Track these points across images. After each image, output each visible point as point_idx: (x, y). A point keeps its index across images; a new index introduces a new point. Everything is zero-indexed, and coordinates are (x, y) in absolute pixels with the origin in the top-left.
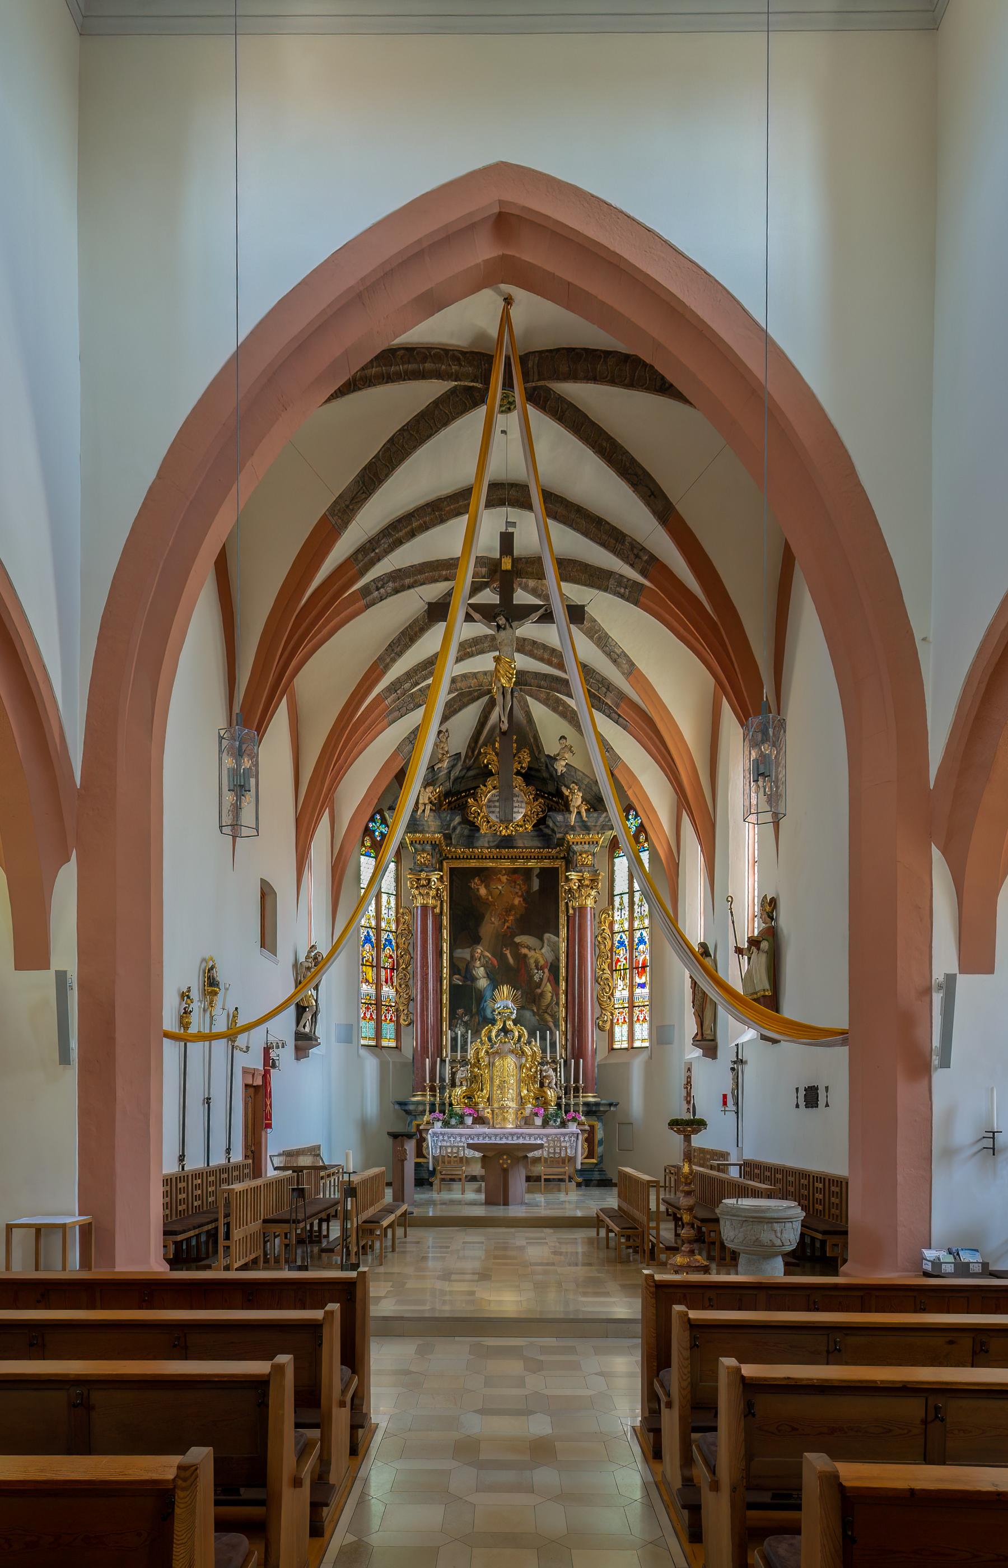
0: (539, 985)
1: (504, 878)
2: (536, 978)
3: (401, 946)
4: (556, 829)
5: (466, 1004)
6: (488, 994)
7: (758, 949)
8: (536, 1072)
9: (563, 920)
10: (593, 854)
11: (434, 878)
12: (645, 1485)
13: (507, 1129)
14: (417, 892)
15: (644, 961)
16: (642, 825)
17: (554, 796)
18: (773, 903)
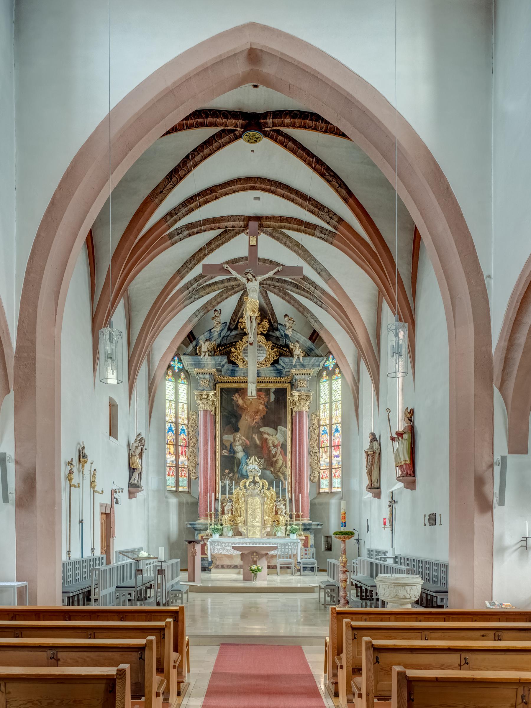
0: (274, 456)
2: (273, 452)
3: (191, 433)
4: (285, 366)
5: (231, 465)
6: (243, 461)
7: (402, 438)
8: (273, 506)
10: (307, 381)
11: (211, 394)
13: (255, 537)
14: (200, 402)
15: (338, 442)
17: (283, 346)
18: (412, 412)
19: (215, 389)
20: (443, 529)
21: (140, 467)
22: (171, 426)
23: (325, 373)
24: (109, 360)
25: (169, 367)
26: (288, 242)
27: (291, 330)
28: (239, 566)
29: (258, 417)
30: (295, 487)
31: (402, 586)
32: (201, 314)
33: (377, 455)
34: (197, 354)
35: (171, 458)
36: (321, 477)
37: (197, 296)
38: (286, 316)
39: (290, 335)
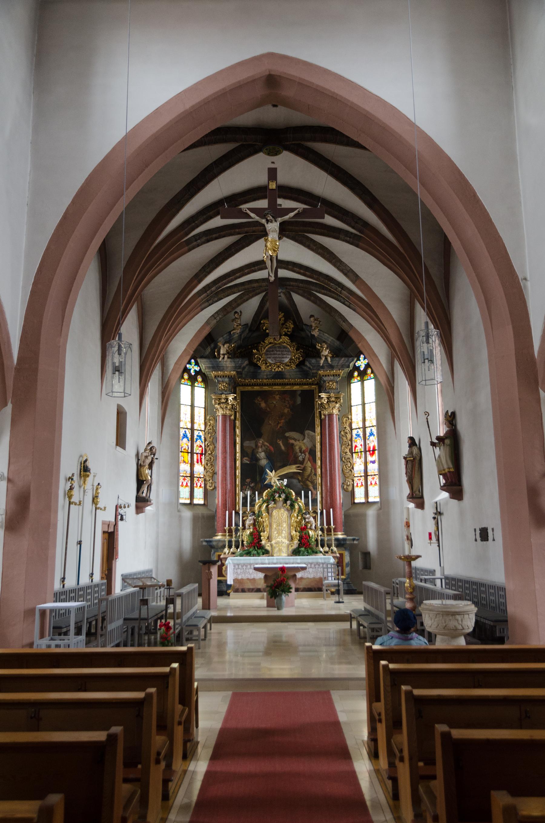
1: (277, 397)
3: (208, 439)
4: (311, 367)
7: (444, 443)
8: (301, 519)
9: (317, 422)
10: (337, 382)
12: (370, 773)
13: (280, 556)
15: (374, 447)
16: (368, 363)
18: (453, 414)
19: (235, 393)
20: (496, 546)
21: (149, 478)
22: (185, 431)
23: (356, 374)
24: (117, 373)
25: (186, 370)
26: (311, 245)
27: (317, 330)
28: (262, 590)
29: (283, 421)
30: (326, 497)
31: (452, 615)
32: (220, 316)
33: (417, 461)
34: (215, 357)
35: (185, 468)
36: (355, 485)
37: (216, 299)
38: (312, 316)
39: (316, 335)
